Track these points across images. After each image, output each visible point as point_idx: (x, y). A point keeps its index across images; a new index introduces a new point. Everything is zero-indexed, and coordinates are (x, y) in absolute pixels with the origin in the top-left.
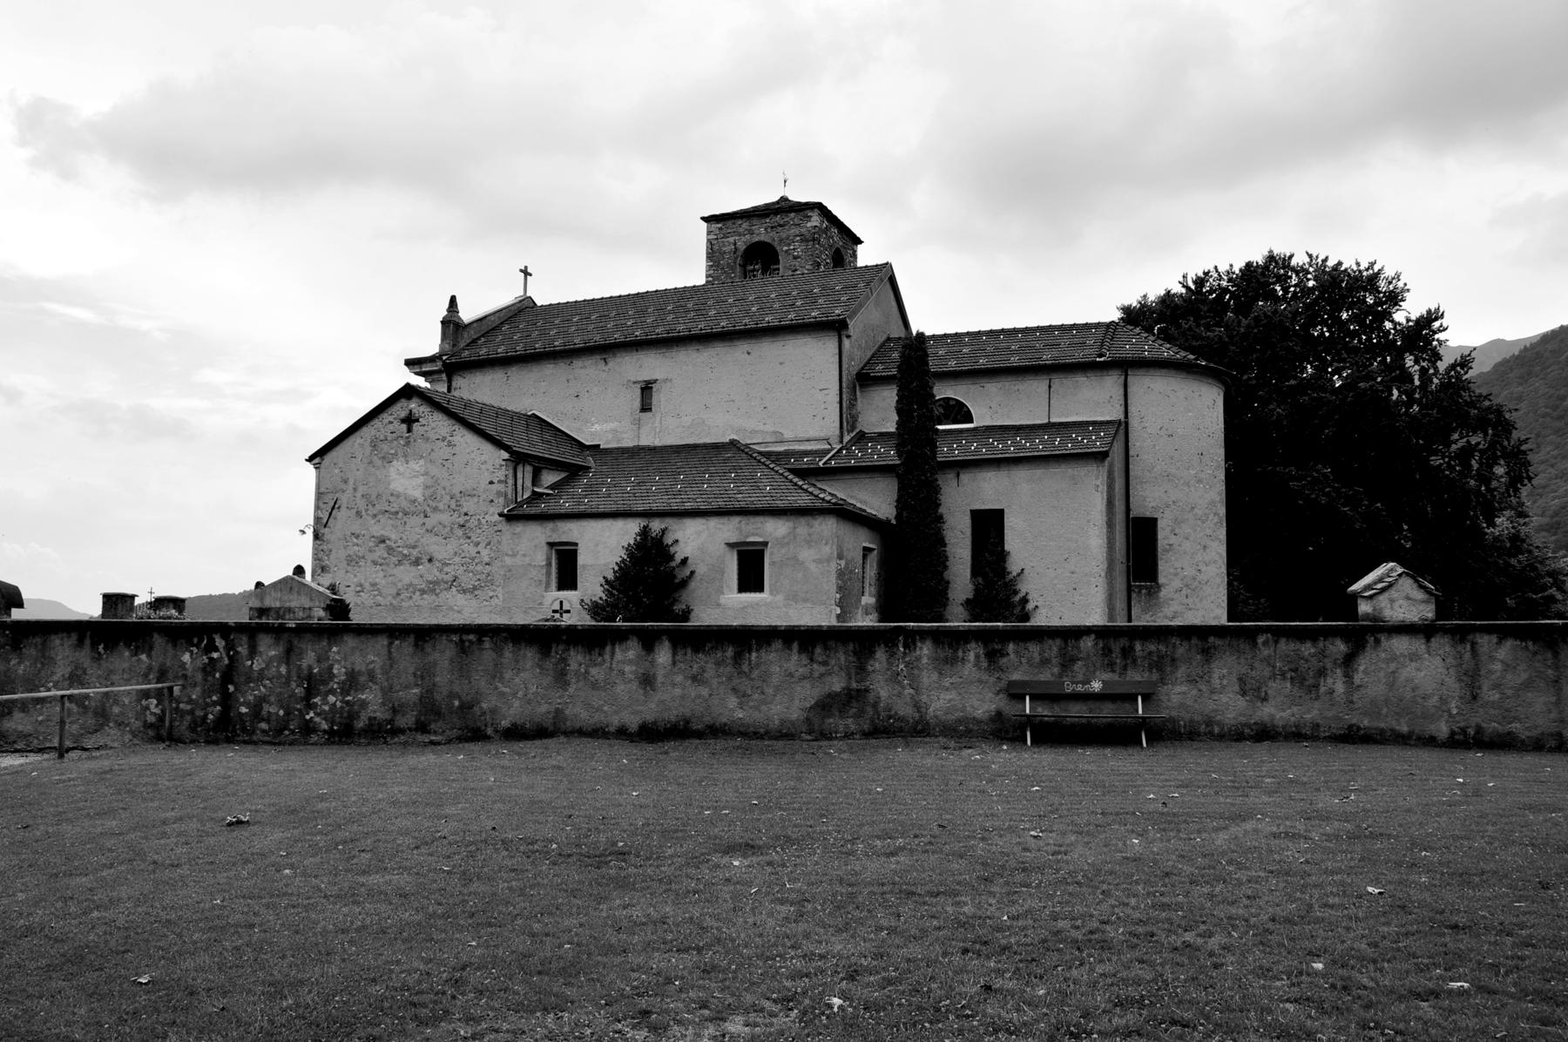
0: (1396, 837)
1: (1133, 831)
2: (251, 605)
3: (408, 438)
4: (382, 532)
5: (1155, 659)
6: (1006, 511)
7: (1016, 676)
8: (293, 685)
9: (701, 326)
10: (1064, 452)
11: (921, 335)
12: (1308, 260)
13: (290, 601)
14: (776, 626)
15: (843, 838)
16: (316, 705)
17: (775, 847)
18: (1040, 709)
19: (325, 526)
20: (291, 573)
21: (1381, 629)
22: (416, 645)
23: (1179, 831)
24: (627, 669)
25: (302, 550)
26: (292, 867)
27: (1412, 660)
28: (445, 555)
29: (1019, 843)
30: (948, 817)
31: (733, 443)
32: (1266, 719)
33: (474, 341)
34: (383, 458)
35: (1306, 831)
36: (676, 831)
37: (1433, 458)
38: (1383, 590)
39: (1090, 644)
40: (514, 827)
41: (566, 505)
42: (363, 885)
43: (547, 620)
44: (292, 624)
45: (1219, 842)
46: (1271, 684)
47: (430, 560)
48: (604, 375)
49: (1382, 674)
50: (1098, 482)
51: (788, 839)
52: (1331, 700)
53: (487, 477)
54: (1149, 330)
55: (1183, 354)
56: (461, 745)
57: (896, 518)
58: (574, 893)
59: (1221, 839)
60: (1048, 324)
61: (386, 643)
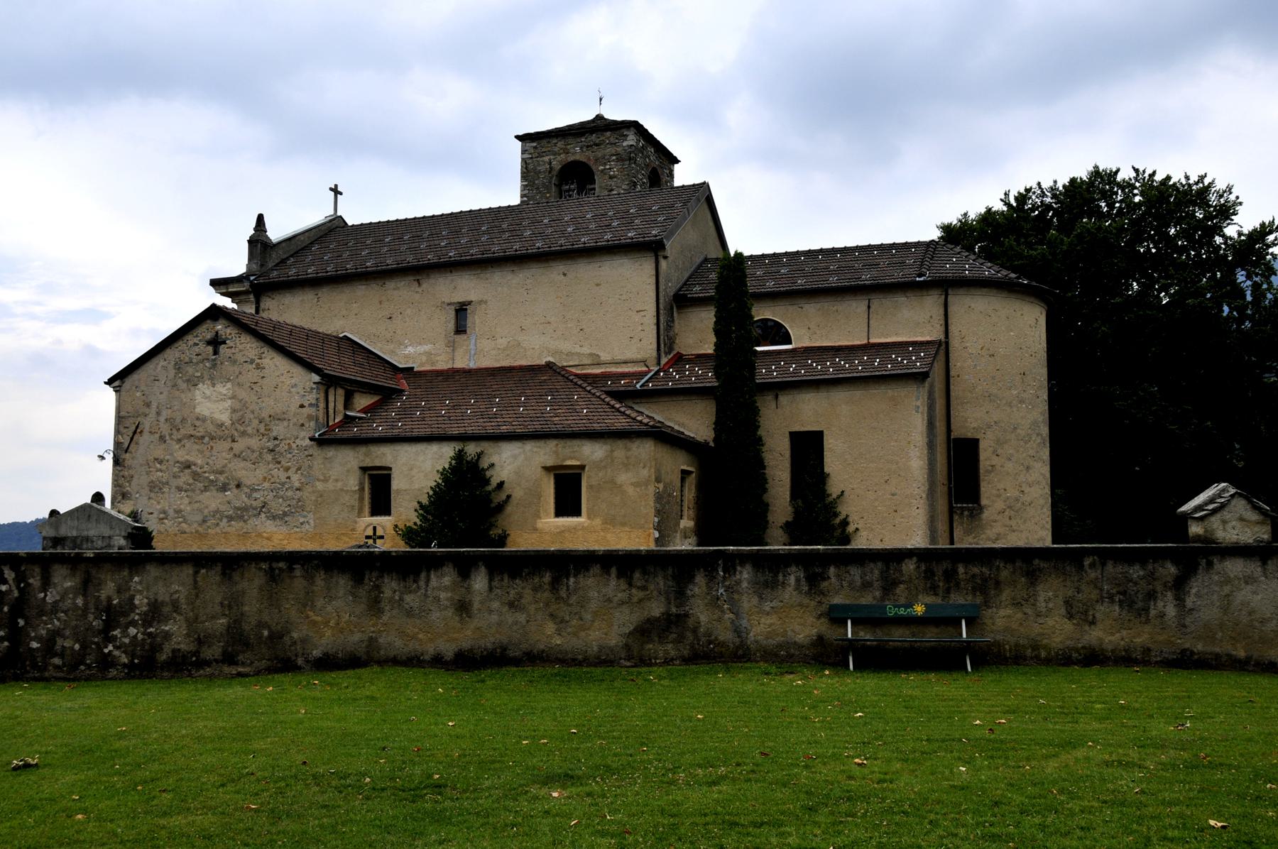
0: (1238, 768)
1: (960, 758)
2: (44, 534)
3: (214, 360)
4: (187, 457)
5: (979, 581)
6: (825, 433)
7: (837, 600)
8: (91, 617)
9: (516, 247)
10: (884, 373)
11: (739, 256)
12: (1135, 175)
13: (87, 530)
14: (594, 551)
15: (664, 767)
16: (115, 638)
17: (595, 778)
18: (862, 634)
19: (126, 452)
20: (89, 501)
21: (1213, 551)
22: (224, 574)
23: (1007, 758)
24: (443, 595)
25: (101, 479)
26: (85, 811)
27: (1247, 583)
28: (254, 481)
29: (844, 771)
30: (771, 744)
31: (549, 365)
32: (1094, 642)
33: (283, 261)
34: (188, 381)
35: (1140, 759)
36: (493, 762)
37: (1267, 375)
38: (1214, 511)
39: (912, 567)
40: (325, 760)
41: (379, 429)
42: (164, 827)
43: (360, 547)
44: (90, 554)
45: (1049, 770)
46: (1098, 607)
47: (238, 486)
48: (417, 297)
49: (1215, 597)
50: (919, 403)
51: (608, 768)
52: (1162, 623)
53: (297, 400)
54: (970, 249)
55: (1004, 272)
56: (270, 677)
57: (715, 440)
58: (388, 829)
59: (1051, 767)
60: (867, 244)
61: (191, 571)
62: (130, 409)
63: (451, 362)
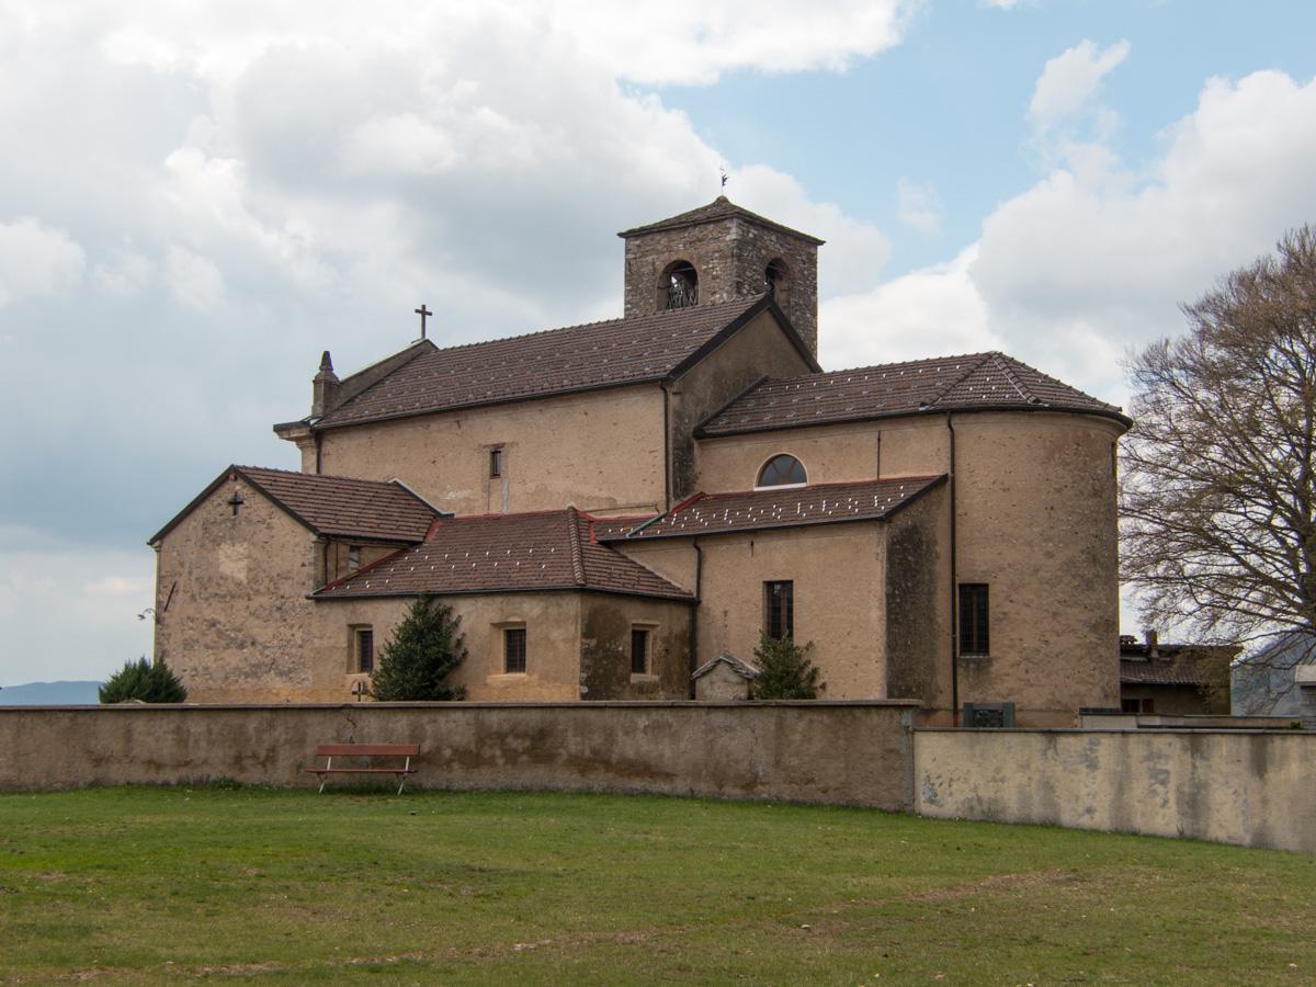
3: (234, 520)
33: (351, 400)
34: (214, 541)
62: (168, 569)
63: (486, 508)
